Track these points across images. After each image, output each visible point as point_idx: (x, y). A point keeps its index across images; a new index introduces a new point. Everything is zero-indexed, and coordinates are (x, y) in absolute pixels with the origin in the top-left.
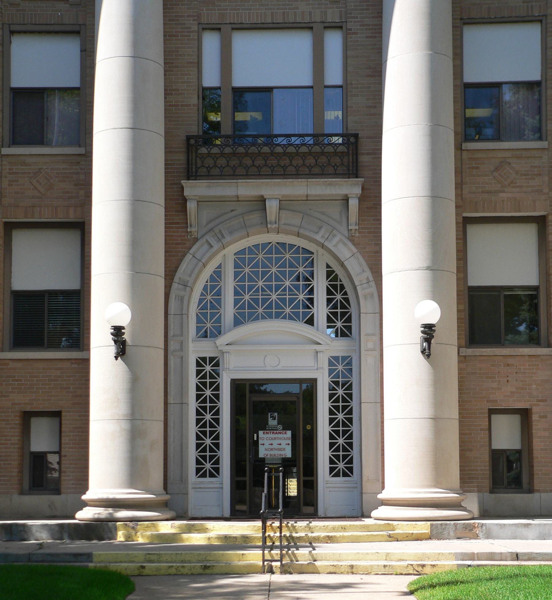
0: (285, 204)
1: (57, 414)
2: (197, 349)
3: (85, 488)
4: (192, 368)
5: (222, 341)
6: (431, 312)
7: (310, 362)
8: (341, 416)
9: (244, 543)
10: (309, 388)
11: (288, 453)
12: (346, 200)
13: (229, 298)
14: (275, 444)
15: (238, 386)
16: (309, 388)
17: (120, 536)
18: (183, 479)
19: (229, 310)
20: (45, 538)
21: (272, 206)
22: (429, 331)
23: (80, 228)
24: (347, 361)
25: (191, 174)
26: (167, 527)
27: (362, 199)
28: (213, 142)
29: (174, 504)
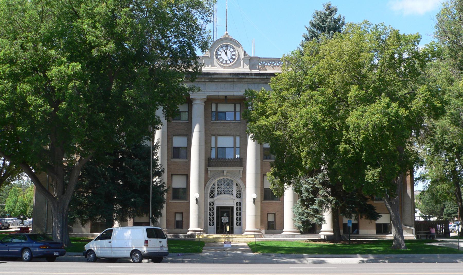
0: (228, 172)
1: (182, 213)
2: (210, 200)
3: (189, 228)
4: (209, 204)
5: (215, 198)
6: (255, 196)
7: (232, 203)
8: (238, 209)
9: (219, 238)
10: (232, 208)
11: (228, 221)
12: (240, 171)
13: (216, 190)
14: (225, 219)
15: (218, 208)
16: (232, 208)
17: (197, 237)
18: (207, 226)
19: (216, 192)
20: (183, 237)
21: (225, 172)
22: (254, 199)
23: (187, 176)
24: (240, 203)
25: (209, 166)
26: (205, 235)
27: (243, 171)
28: (215, 161)
29: (206, 231)
